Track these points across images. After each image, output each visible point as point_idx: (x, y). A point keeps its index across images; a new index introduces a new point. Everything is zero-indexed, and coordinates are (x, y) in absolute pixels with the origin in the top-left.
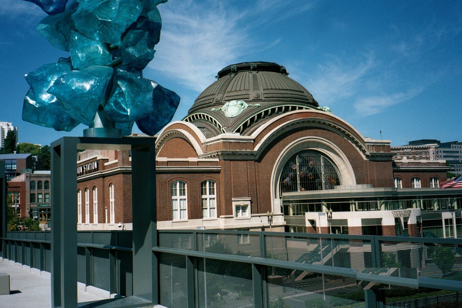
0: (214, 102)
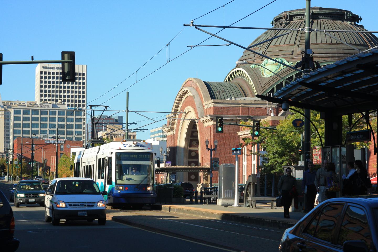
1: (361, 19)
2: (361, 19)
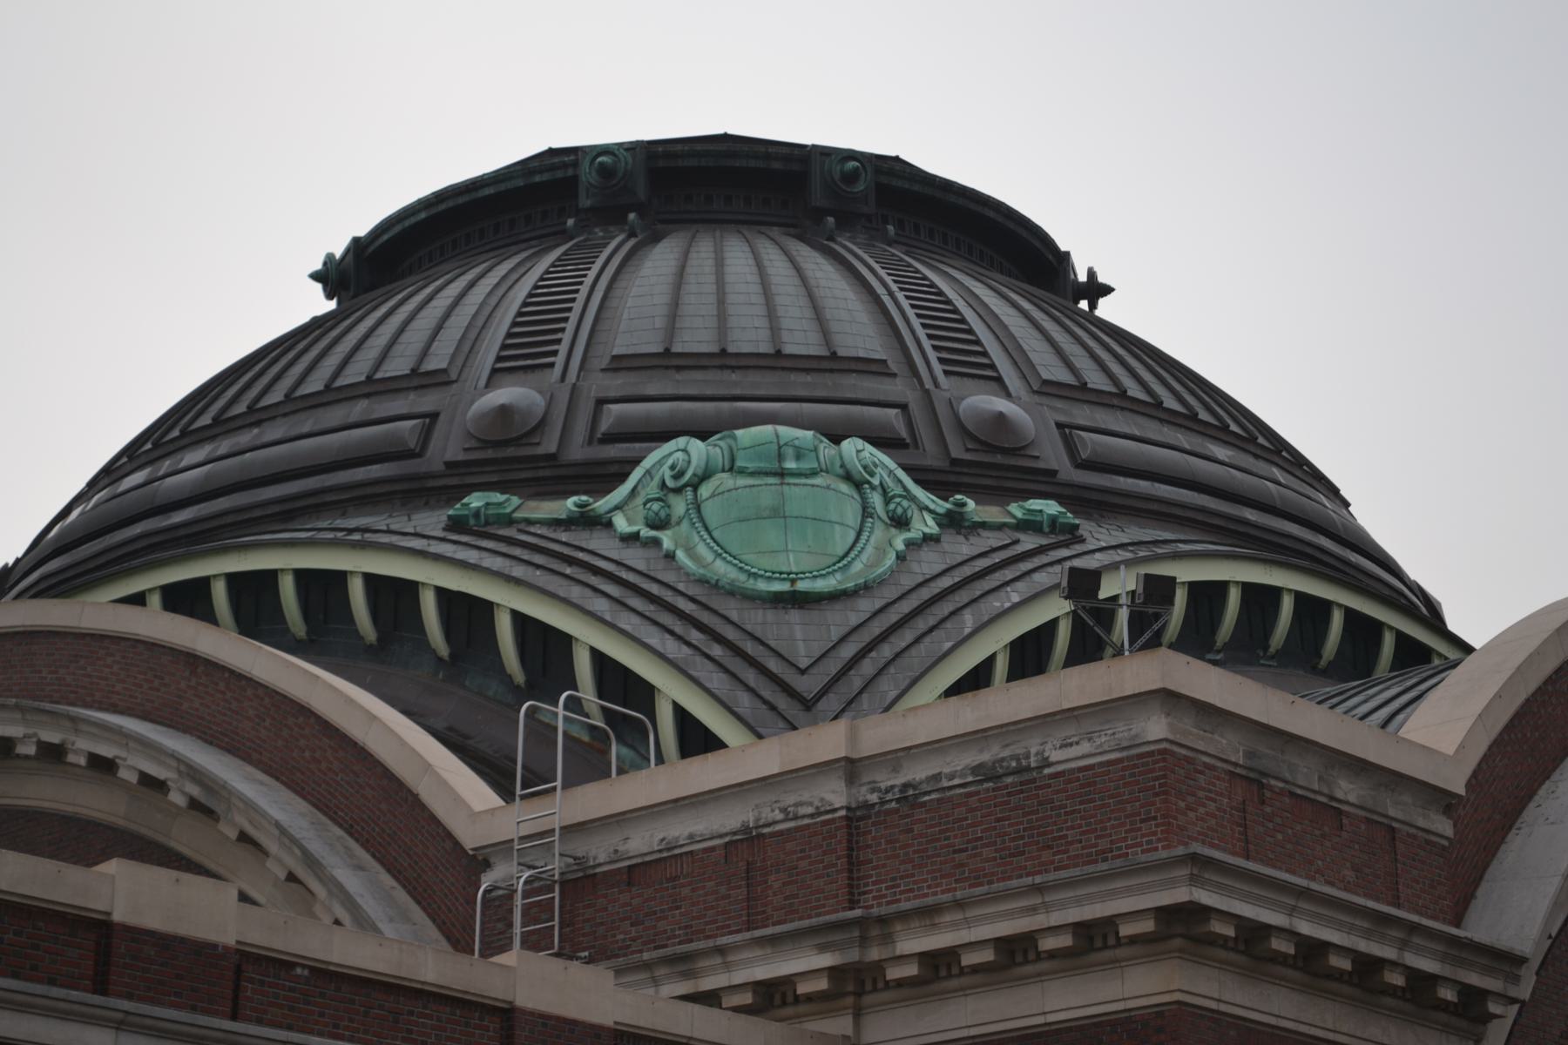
0: (448, 446)
1: (1096, 290)
2: (1096, 290)
